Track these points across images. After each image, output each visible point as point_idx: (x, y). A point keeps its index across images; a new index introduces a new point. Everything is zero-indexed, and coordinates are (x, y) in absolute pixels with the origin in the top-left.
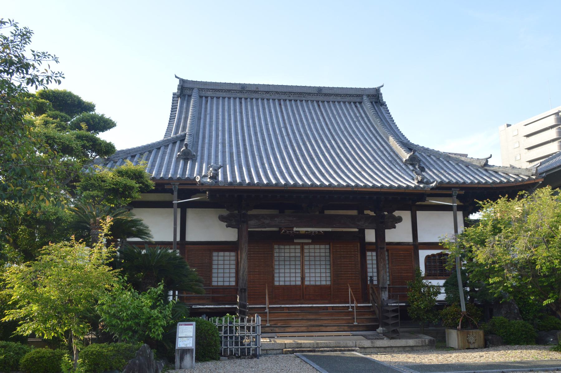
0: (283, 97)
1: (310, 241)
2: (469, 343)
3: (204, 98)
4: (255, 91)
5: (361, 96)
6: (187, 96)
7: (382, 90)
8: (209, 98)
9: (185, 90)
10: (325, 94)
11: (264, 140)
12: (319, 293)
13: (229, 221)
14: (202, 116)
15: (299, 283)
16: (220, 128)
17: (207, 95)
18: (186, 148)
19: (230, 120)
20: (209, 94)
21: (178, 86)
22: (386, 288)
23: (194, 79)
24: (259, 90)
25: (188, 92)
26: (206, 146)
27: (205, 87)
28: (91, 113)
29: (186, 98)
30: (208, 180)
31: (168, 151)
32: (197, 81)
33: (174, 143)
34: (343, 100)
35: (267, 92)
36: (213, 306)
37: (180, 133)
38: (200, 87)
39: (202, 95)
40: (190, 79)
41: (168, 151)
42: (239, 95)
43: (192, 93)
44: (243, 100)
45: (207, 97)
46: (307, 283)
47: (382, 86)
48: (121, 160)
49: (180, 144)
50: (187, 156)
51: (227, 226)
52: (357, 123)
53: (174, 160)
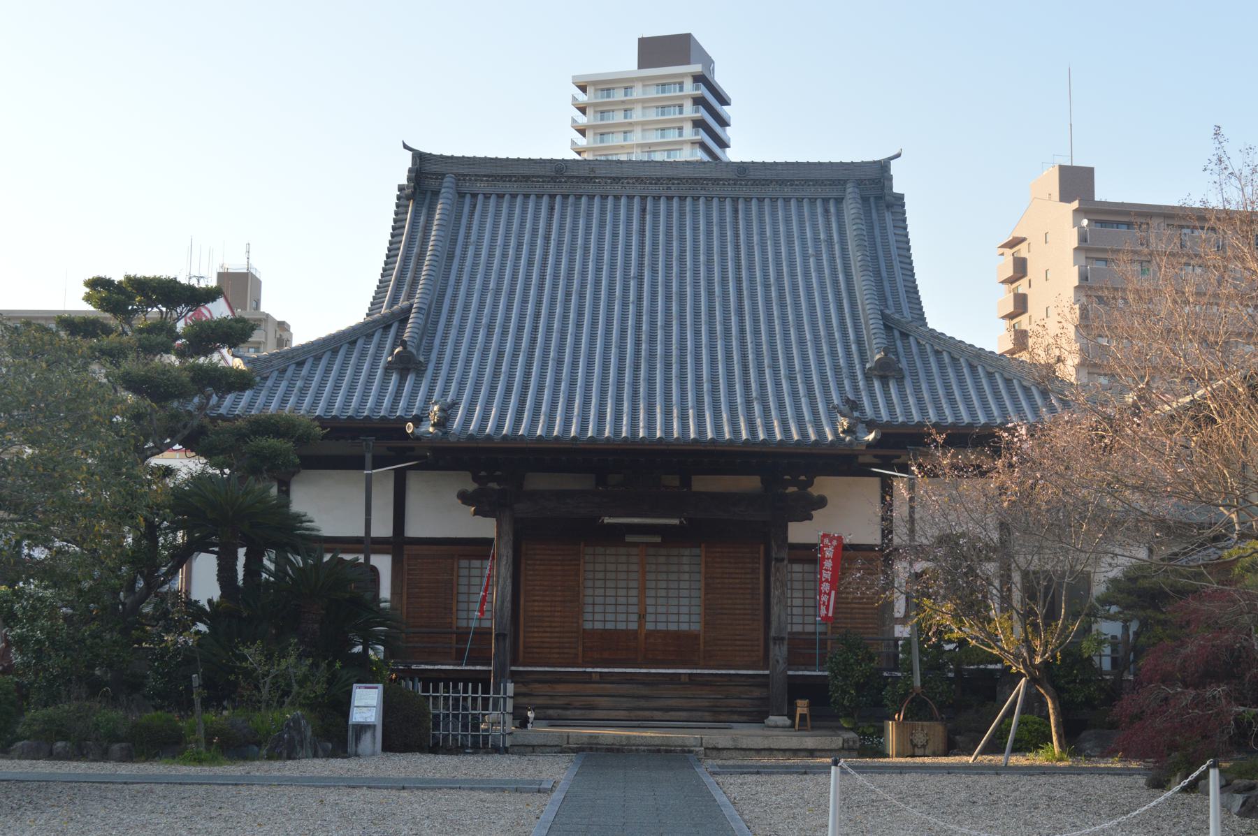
0: (654, 190)
1: (659, 540)
2: (914, 746)
3: (468, 197)
4: (586, 178)
5: (841, 183)
6: (429, 194)
7: (895, 167)
8: (480, 197)
9: (428, 180)
10: (755, 180)
11: (580, 314)
12: (678, 647)
13: (479, 502)
14: (458, 252)
15: (633, 626)
16: (492, 285)
17: (475, 190)
18: (405, 348)
19: (517, 258)
20: (481, 187)
21: (410, 171)
22: (783, 639)
23: (447, 153)
24: (597, 174)
25: (432, 184)
26: (453, 333)
27: (471, 171)
28: (202, 360)
29: (427, 201)
30: (431, 429)
31: (372, 349)
32: (452, 157)
33: (387, 328)
34: (797, 194)
35: (616, 180)
36: (451, 667)
37: (402, 303)
38: (461, 171)
39: (464, 189)
40: (436, 151)
41: (372, 349)
42: (549, 188)
43: (441, 185)
44: (558, 199)
45: (474, 196)
46: (650, 626)
47: (898, 156)
48: (275, 374)
49: (397, 332)
50: (406, 365)
51: (476, 513)
52: (811, 260)
53: (380, 372)
